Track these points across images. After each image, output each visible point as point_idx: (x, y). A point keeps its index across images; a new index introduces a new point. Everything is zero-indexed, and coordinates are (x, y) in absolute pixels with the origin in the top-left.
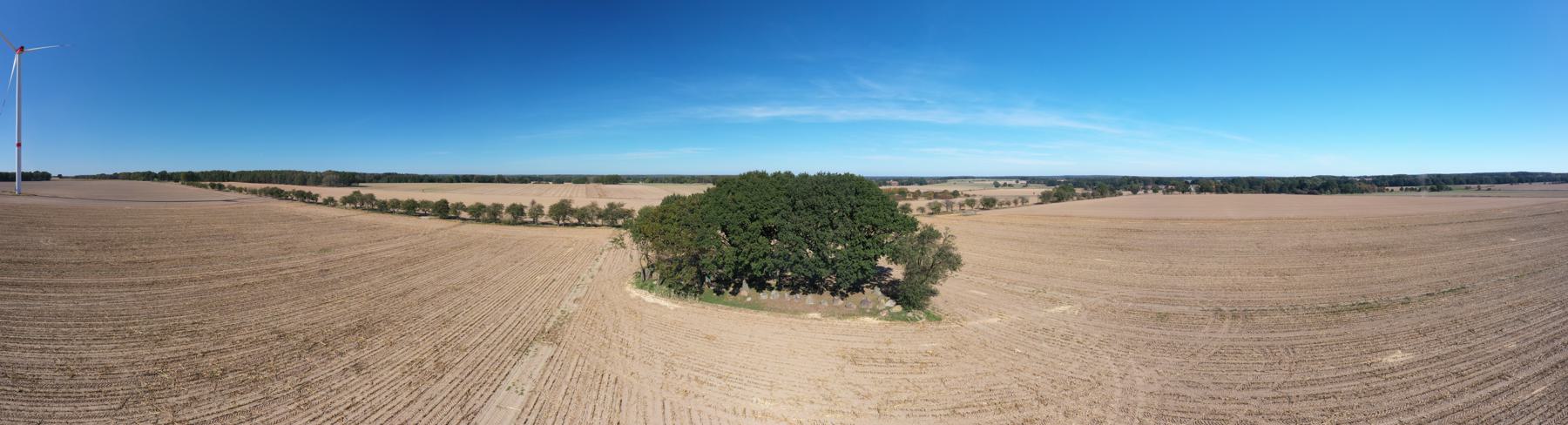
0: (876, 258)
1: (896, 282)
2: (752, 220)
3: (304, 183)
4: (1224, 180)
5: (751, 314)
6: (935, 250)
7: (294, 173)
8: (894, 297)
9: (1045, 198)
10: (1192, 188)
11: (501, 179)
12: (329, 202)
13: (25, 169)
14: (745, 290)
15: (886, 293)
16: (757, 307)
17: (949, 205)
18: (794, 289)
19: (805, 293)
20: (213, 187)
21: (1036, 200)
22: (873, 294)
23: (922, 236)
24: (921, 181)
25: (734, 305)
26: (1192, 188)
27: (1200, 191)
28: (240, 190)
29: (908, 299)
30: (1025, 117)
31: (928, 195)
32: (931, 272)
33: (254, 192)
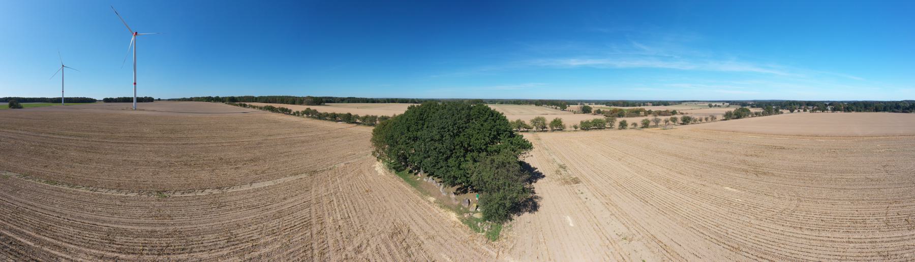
3: (287, 103)
4: (849, 103)
7: (276, 97)
9: (728, 116)
10: (829, 108)
11: (373, 101)
12: (297, 114)
13: (139, 95)
17: (657, 121)
20: (241, 105)
21: (721, 117)
26: (829, 108)
27: (834, 110)
28: (254, 107)
30: (732, 66)
33: (261, 108)
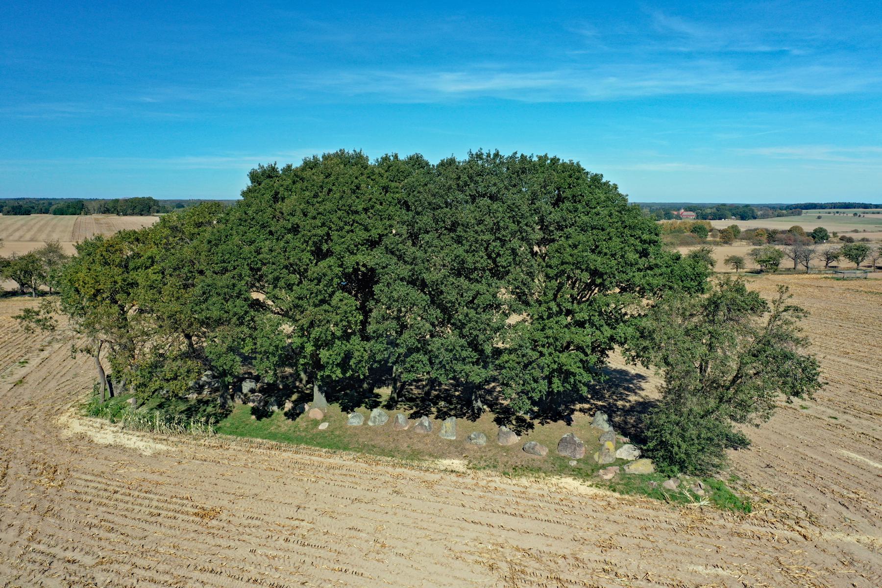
0: (601, 349)
1: (645, 406)
2: (320, 254)
5: (320, 457)
6: (743, 342)
8: (638, 439)
14: (318, 408)
15: (621, 429)
16: (334, 442)
18: (421, 407)
19: (442, 415)
22: (589, 426)
23: (714, 304)
24: (745, 212)
25: (288, 438)
29: (671, 444)
32: (730, 393)
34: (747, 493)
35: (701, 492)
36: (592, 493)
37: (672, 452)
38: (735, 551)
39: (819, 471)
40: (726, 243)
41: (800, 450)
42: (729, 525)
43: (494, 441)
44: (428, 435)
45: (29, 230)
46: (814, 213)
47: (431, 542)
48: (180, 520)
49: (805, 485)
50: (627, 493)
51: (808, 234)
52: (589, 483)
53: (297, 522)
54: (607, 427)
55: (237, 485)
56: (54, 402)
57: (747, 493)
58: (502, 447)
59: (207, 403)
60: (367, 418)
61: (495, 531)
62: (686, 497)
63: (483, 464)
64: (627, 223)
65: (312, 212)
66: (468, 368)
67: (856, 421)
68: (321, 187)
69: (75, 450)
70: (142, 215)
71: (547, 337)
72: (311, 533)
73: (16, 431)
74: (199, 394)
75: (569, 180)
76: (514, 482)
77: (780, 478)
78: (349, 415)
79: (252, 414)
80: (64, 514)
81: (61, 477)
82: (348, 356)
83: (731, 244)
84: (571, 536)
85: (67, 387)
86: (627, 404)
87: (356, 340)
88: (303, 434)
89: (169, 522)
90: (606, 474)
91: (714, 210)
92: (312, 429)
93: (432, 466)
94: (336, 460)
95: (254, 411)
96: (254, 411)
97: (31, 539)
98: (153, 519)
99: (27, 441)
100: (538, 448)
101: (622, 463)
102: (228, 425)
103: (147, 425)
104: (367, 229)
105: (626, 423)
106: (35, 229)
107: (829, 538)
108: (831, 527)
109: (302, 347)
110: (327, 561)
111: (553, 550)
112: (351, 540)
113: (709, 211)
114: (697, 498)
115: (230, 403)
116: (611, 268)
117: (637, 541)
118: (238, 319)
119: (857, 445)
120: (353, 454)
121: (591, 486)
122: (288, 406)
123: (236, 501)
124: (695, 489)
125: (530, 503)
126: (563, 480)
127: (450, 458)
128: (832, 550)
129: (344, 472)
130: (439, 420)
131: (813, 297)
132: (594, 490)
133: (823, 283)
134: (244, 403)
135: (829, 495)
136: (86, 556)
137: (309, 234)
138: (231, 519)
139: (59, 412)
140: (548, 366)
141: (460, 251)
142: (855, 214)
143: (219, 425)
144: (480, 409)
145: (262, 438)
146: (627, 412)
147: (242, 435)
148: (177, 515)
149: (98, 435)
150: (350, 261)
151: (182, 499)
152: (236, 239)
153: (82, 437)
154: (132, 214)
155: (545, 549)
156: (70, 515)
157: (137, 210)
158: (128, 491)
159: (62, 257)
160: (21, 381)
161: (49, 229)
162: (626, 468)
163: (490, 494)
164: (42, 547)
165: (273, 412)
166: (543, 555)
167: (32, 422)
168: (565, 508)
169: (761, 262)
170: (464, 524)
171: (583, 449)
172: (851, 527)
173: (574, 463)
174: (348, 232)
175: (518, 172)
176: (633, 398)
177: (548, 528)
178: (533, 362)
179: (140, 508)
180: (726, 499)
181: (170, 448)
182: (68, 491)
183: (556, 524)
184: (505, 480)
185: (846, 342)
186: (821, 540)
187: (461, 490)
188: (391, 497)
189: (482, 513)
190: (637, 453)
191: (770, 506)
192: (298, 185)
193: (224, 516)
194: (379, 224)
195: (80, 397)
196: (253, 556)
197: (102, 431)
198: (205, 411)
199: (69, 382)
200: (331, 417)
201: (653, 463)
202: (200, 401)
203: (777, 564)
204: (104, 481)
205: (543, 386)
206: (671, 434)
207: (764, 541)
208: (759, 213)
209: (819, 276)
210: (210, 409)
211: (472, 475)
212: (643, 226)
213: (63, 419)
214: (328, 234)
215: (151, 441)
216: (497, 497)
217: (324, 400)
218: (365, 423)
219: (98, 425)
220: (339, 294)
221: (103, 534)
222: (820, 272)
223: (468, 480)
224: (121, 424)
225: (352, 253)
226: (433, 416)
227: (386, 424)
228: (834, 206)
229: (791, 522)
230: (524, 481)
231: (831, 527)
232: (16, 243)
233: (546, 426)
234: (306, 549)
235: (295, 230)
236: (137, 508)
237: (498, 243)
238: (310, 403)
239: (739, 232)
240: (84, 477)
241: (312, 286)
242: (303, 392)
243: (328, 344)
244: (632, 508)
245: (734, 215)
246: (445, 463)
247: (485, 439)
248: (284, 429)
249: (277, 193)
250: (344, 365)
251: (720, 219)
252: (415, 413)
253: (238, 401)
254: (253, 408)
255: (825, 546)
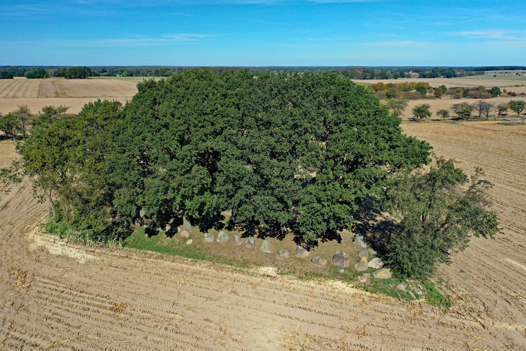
2: (182, 142)
5: (186, 265)
8: (382, 252)
14: (186, 230)
15: (372, 243)
16: (196, 254)
19: (262, 235)
23: (432, 178)
24: (449, 73)
29: (402, 251)
31: (456, 93)
34: (449, 293)
35: (420, 293)
36: (353, 292)
37: (403, 268)
38: (441, 337)
39: (493, 275)
40: (437, 97)
41: (482, 258)
42: (438, 317)
43: (293, 254)
44: (253, 249)
45: (12, 90)
46: (492, 73)
47: (254, 330)
48: (101, 313)
49: (483, 286)
50: (375, 292)
51: (488, 91)
52: (351, 285)
53: (172, 315)
54: (364, 245)
55: (136, 287)
56: (26, 223)
57: (449, 293)
58: (299, 259)
59: (118, 224)
60: (216, 237)
61: (294, 322)
62: (411, 296)
63: (287, 270)
64: (379, 121)
65: (178, 115)
66: (277, 214)
67: (515, 235)
68: (183, 97)
69: (38, 259)
70: (81, 78)
71: (327, 196)
72: (181, 323)
73: (2, 245)
74: (113, 217)
75: (343, 92)
76: (306, 284)
77: (470, 281)
78: (206, 235)
79: (146, 233)
80: (30, 309)
81: (29, 280)
82: (203, 204)
83: (440, 98)
84: (340, 326)
85: (34, 211)
86: (375, 223)
87: (207, 194)
88: (177, 247)
89: (95, 315)
90: (362, 279)
91: (431, 72)
92: (183, 243)
93: (255, 272)
94: (197, 267)
95: (147, 231)
96: (147, 231)
97: (10, 328)
98: (84, 313)
99: (9, 253)
100: (320, 261)
101: (372, 270)
102: (132, 241)
103: (80, 241)
104: (213, 124)
105: (374, 237)
106: (16, 89)
107: (498, 327)
108: (499, 318)
109: (174, 198)
110: (190, 346)
111: (329, 336)
112: (206, 329)
113: (427, 72)
114: (417, 296)
115: (132, 225)
116: (368, 152)
117: (380, 329)
118: (133, 184)
119: (517, 255)
120: (208, 263)
121: (353, 287)
122: (168, 228)
123: (136, 299)
124: (416, 291)
125: (316, 300)
126: (336, 283)
127: (267, 266)
128: (500, 336)
129: (202, 276)
130: (260, 239)
131: (490, 138)
132: (355, 290)
133: (496, 128)
134: (141, 225)
135: (499, 294)
136: (44, 341)
137: (176, 130)
138: (133, 312)
139: (29, 230)
140: (327, 214)
141: (272, 141)
142: (517, 74)
143: (126, 240)
144: (285, 232)
145: (152, 250)
146: (375, 229)
147: (140, 248)
148: (100, 310)
149: (52, 247)
150: (202, 146)
151: (103, 297)
152: (130, 131)
153: (42, 249)
154: (75, 78)
155: (325, 336)
156: (34, 309)
157: (77, 75)
158: (70, 291)
159: (30, 115)
160: (6, 206)
161: (24, 89)
162: (374, 274)
163: (290, 293)
164: (17, 334)
165: (158, 232)
166: (322, 340)
167: (12, 238)
168: (337, 304)
169: (459, 113)
170: (275, 317)
171: (349, 261)
172: (512, 319)
173: (342, 271)
174: (200, 127)
175: (309, 87)
176: (379, 218)
177: (326, 319)
178: (318, 211)
179: (78, 304)
180: (436, 297)
181: (96, 258)
182: (33, 293)
183: (331, 317)
184: (300, 282)
185: (511, 174)
186: (493, 328)
187: (273, 290)
188: (230, 296)
189: (287, 308)
190: (381, 264)
191: (462, 302)
192: (169, 95)
193: (128, 310)
194: (220, 120)
195: (42, 218)
196: (145, 341)
197: (55, 245)
198: (116, 230)
199: (35, 207)
200: (194, 235)
201: (391, 271)
202: (114, 223)
203: (466, 347)
204: (55, 283)
205: (324, 225)
206: (403, 257)
207: (458, 329)
208: (458, 73)
209: (494, 122)
210: (120, 229)
211: (280, 279)
212: (389, 122)
213: (31, 235)
214: (188, 129)
215: (85, 252)
216: (295, 295)
217: (190, 224)
218: (215, 240)
219: (52, 240)
220: (196, 167)
221: (54, 324)
222: (495, 120)
223: (277, 283)
224: (66, 240)
225: (203, 141)
226: (256, 236)
227: (227, 241)
228: (505, 68)
229: (474, 315)
230: (312, 283)
231: (499, 318)
232: (4, 99)
233: (325, 243)
234: (178, 336)
235: (166, 126)
236: (75, 304)
237: (296, 136)
238: (181, 226)
239: (446, 90)
240: (43, 280)
241: (179, 163)
242: (177, 217)
243: (191, 198)
244: (377, 304)
245: (442, 75)
246: (264, 270)
247: (288, 253)
248: (165, 243)
249: (155, 99)
250: (200, 210)
251: (434, 77)
252: (245, 233)
253: (137, 224)
254: (146, 229)
255: (496, 333)
